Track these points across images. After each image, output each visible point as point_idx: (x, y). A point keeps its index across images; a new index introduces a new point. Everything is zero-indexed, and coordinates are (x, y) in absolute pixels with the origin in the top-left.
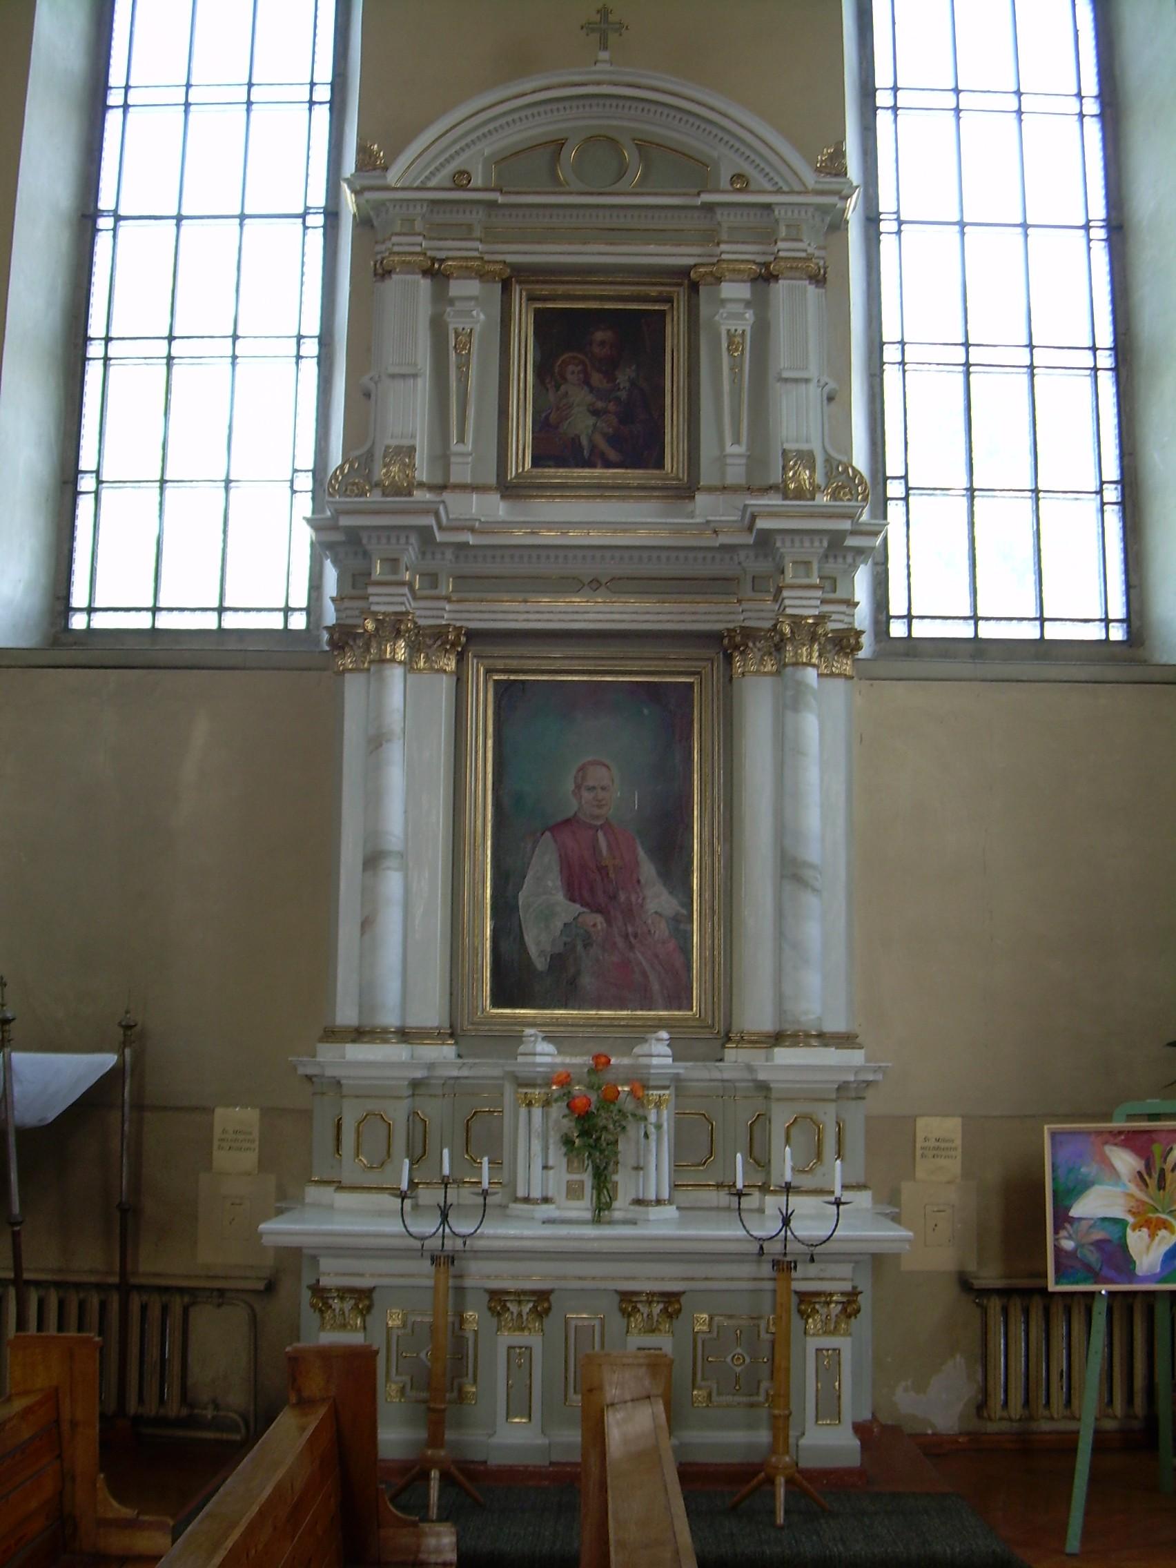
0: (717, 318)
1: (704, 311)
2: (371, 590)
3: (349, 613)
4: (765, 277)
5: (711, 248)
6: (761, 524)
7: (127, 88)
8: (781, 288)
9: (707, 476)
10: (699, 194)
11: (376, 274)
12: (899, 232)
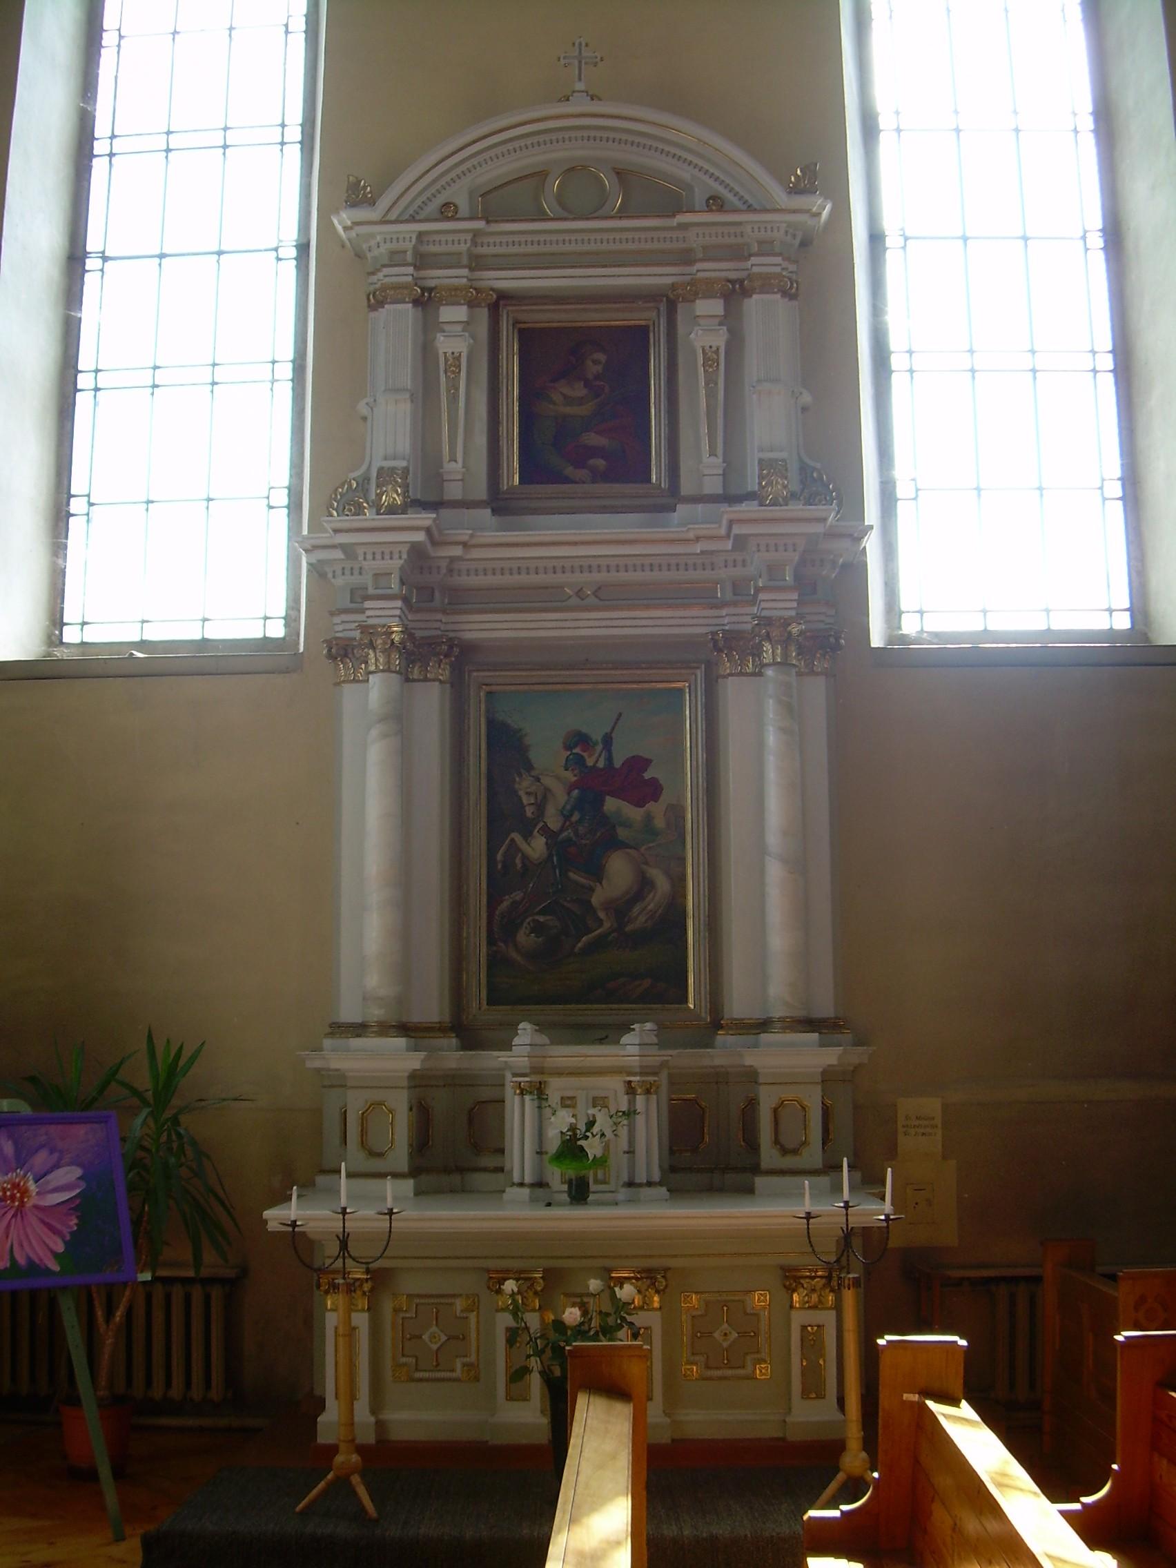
0: (692, 336)
1: (681, 330)
2: (368, 604)
3: (348, 626)
4: (735, 293)
5: (687, 269)
6: (736, 530)
7: (113, 137)
8: (754, 305)
9: (686, 488)
10: (674, 216)
11: (369, 306)
12: (904, 248)
